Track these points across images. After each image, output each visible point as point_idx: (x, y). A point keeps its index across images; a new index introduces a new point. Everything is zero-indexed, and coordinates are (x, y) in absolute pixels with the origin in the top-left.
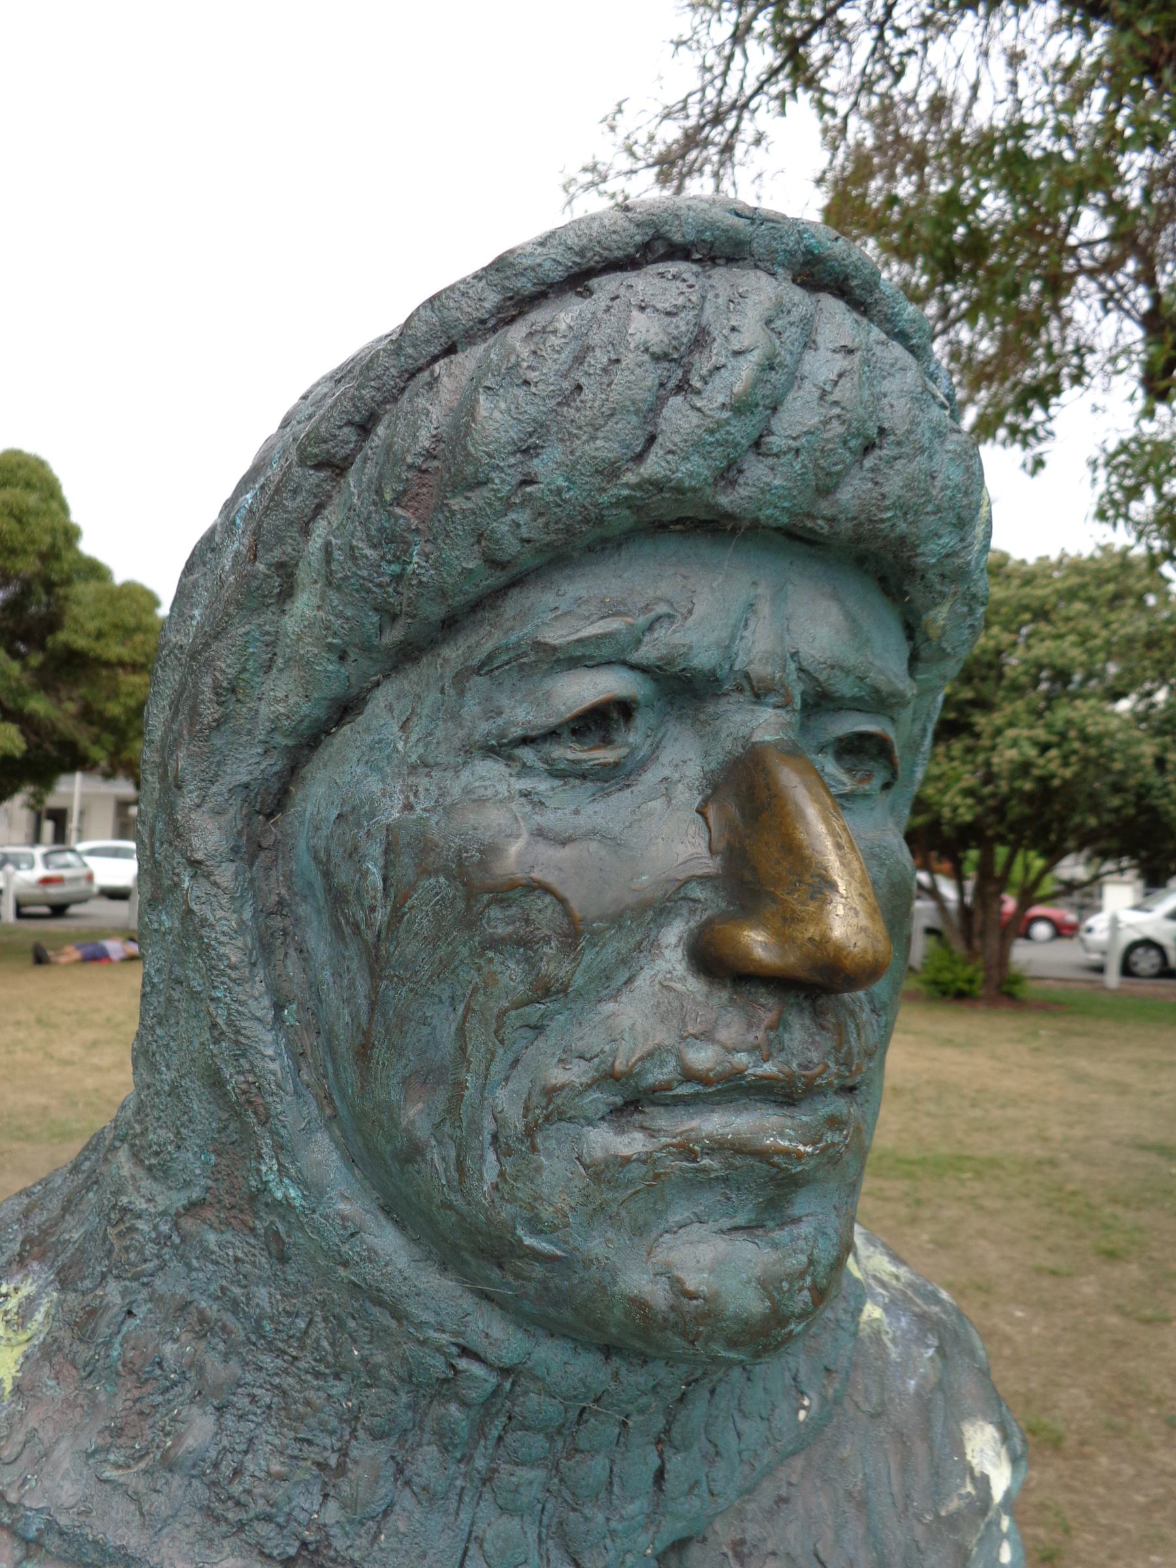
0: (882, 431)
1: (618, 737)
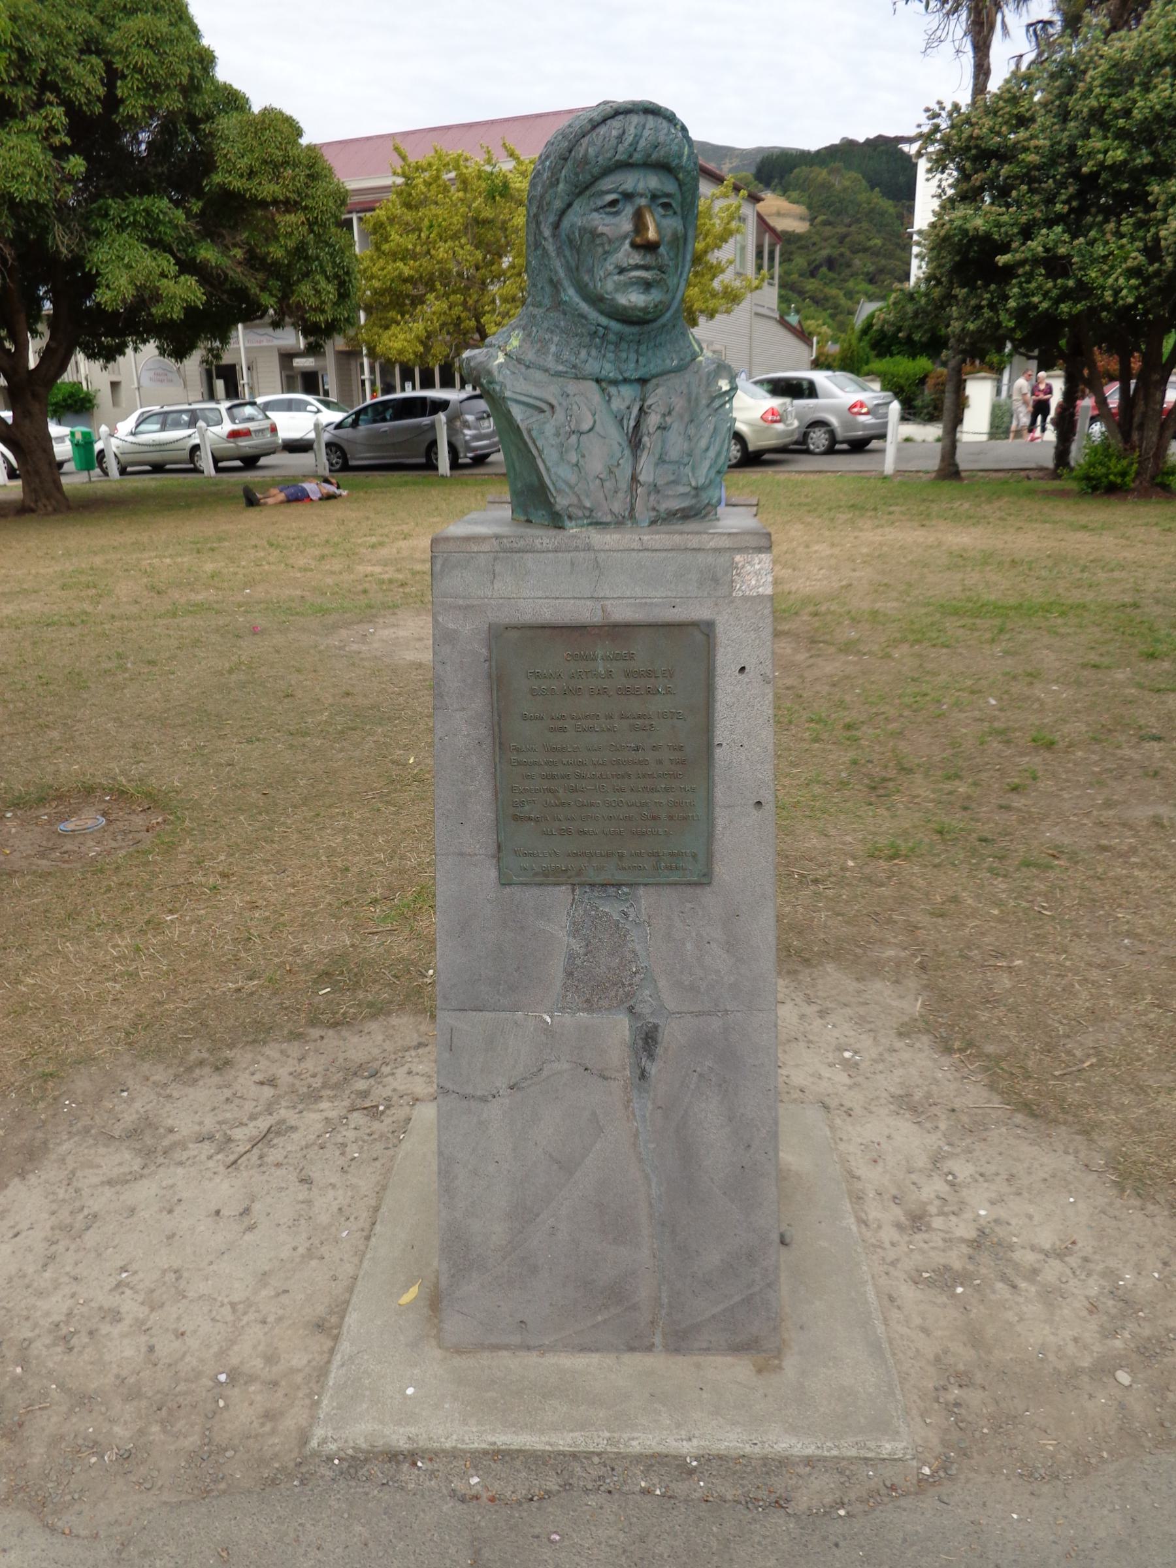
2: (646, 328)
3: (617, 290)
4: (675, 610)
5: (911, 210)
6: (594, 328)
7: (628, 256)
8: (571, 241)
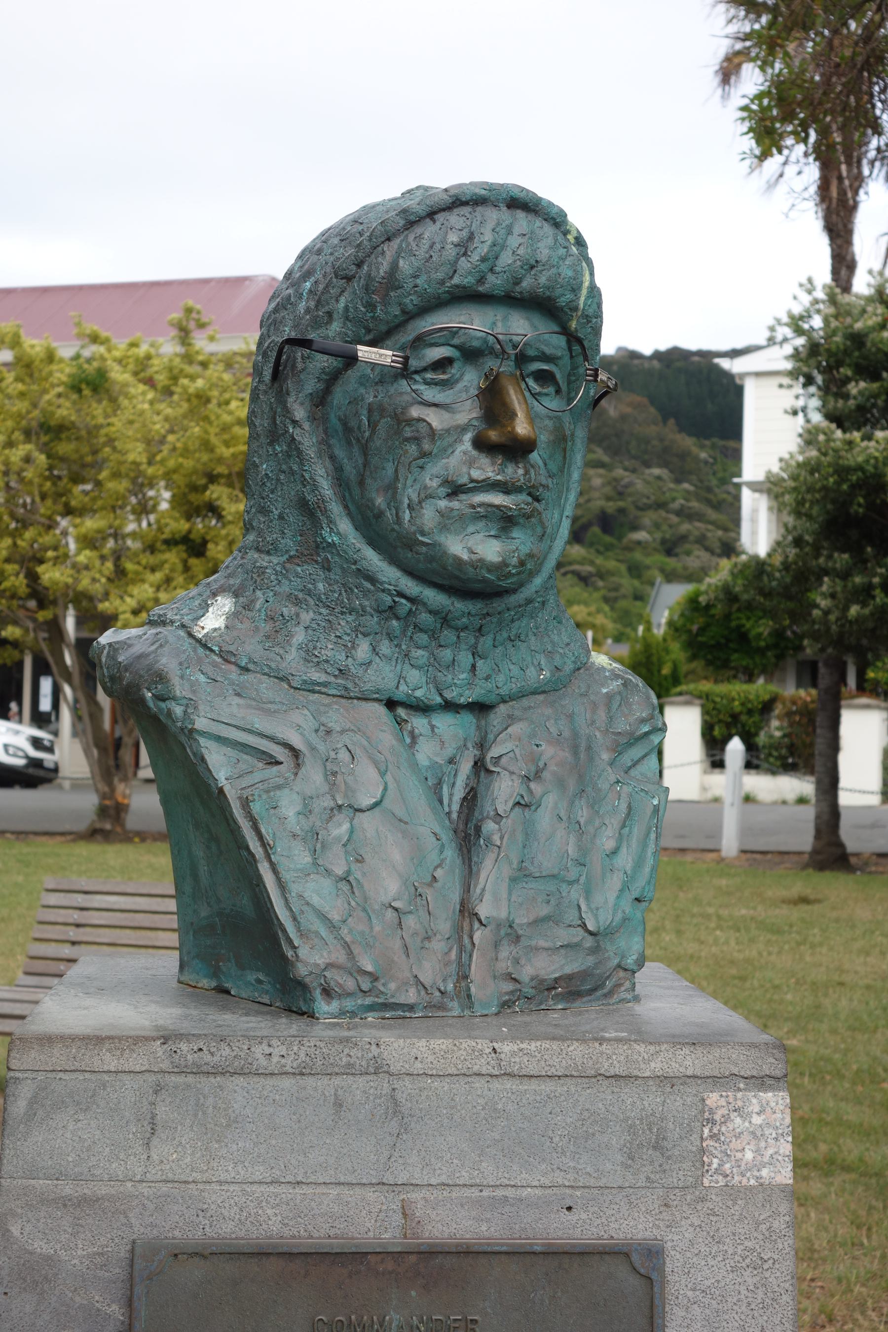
0: (537, 262)
1: (448, 371)
3: (444, 528)
4: (572, 1217)
5: (736, 455)
6: (388, 600)
7: (471, 463)
8: (347, 429)
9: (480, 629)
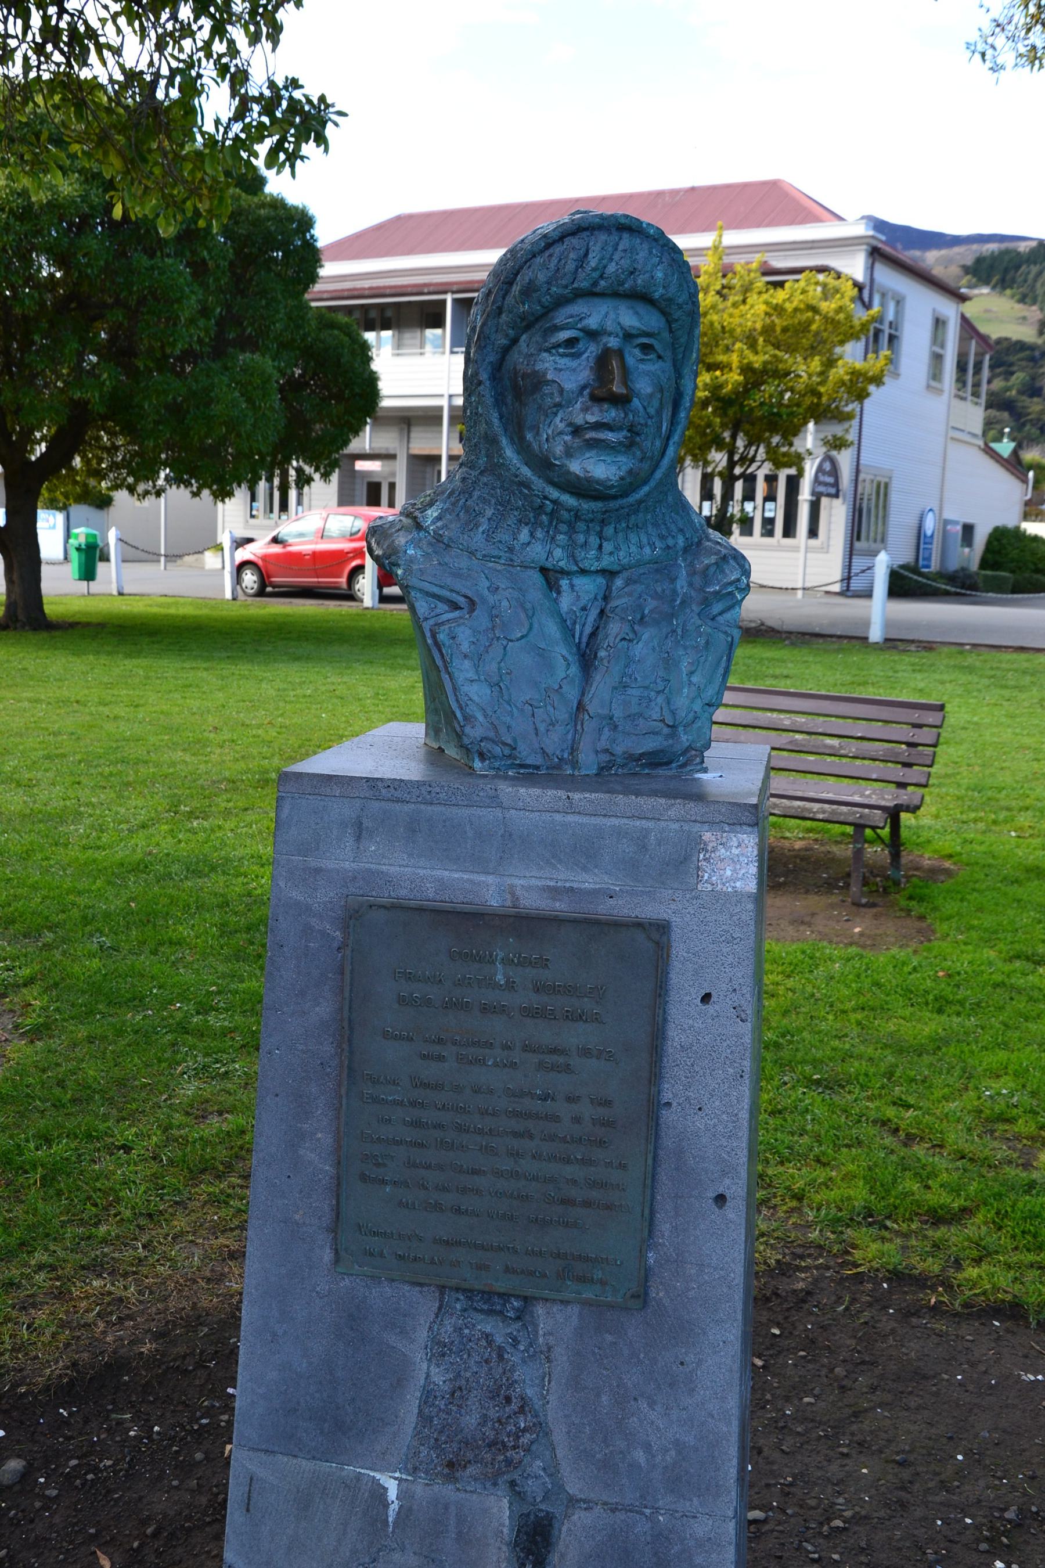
2: (613, 504)
9: (603, 521)
